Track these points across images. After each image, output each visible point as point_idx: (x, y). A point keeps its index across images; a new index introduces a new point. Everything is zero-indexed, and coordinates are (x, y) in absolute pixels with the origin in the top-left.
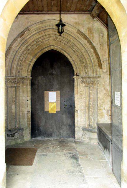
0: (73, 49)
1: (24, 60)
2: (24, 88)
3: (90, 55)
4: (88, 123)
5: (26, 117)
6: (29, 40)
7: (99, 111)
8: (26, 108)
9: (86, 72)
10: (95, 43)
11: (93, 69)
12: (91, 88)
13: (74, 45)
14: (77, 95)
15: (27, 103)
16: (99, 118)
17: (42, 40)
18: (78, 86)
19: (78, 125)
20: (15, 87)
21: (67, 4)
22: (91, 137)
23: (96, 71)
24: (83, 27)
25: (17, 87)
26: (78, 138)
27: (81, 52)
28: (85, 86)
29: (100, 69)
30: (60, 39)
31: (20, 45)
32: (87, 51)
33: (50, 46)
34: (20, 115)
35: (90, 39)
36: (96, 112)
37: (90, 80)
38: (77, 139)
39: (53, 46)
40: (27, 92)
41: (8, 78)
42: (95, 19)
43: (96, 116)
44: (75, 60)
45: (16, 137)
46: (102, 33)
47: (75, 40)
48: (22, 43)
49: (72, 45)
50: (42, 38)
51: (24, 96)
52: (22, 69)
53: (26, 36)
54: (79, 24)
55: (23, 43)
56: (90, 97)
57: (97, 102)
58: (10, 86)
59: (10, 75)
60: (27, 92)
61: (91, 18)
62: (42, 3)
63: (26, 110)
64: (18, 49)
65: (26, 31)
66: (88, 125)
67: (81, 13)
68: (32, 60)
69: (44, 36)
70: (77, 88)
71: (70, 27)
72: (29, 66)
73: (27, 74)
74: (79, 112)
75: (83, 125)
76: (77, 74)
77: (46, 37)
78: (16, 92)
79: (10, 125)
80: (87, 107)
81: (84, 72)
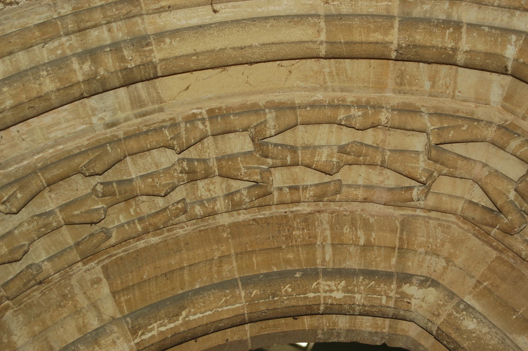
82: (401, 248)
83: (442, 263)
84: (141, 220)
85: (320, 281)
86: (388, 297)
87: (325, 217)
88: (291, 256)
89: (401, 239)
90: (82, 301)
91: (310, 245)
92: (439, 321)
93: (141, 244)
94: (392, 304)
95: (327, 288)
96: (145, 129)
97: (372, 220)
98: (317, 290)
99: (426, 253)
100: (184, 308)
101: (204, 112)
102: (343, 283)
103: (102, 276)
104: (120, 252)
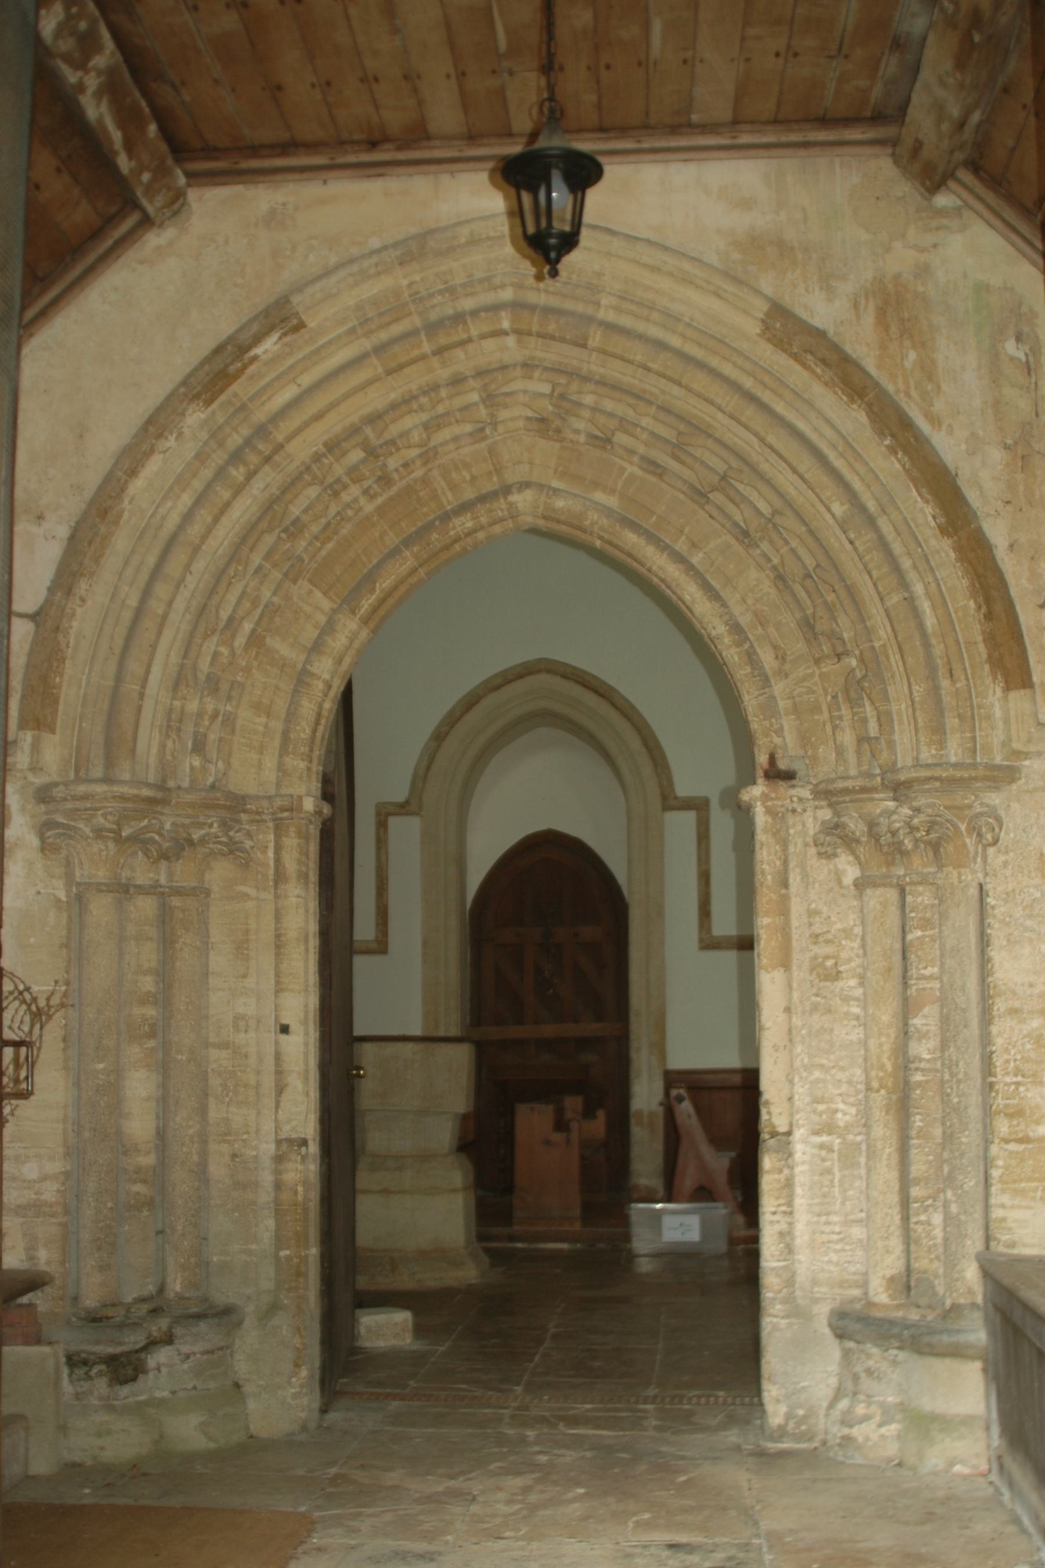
0: (731, 509)
1: (247, 627)
2: (250, 904)
3: (906, 564)
4: (892, 1264)
5: (265, 1196)
6: (287, 426)
7: (1003, 1126)
8: (269, 1102)
9: (862, 739)
10: (950, 430)
11: (939, 702)
12: (922, 898)
13: (735, 463)
14: (778, 975)
15: (278, 1056)
16: (1005, 1199)
17: (426, 426)
18: (785, 884)
19: (790, 1282)
20: (152, 889)
21: (646, 27)
22: (928, 1404)
23: (969, 720)
24: (827, 283)
25: (179, 892)
26: (789, 1416)
27: (811, 532)
28: (860, 885)
29: (1007, 689)
30: (602, 420)
31: (207, 473)
32: (871, 522)
33: (506, 490)
34: (201, 1172)
35: (902, 400)
36: (969, 1139)
37: (906, 811)
38: (781, 1433)
39: (529, 495)
40: (279, 944)
41: (82, 789)
42: (943, 200)
43: (971, 1183)
44: (761, 620)
45: (166, 1394)
46: (1019, 339)
47: (749, 412)
48: (219, 458)
49: (721, 467)
50: (421, 408)
51: (250, 982)
52: (229, 722)
53: (264, 389)
54: (783, 248)
55: (236, 457)
56: (912, 991)
57: (986, 1039)
58: (102, 875)
59: (110, 762)
60: (279, 944)
61: (905, 188)
62: (395, 31)
63: (268, 1126)
64: (188, 517)
65: (257, 340)
66: (892, 1280)
67: (794, 137)
68: (329, 628)
69: (443, 393)
70: (783, 909)
71: (687, 281)
72: (296, 691)
73: (280, 767)
74: (802, 1148)
75: (842, 1284)
76: (782, 765)
77: (459, 402)
78: (167, 943)
79: (103, 1268)
80: (879, 1099)
81: (847, 738)
82: (495, 470)
83: (527, 467)
84: (316, 538)
85: (453, 520)
86: (502, 510)
87: (435, 473)
88: (425, 510)
89: (493, 464)
90: (308, 609)
91: (435, 497)
92: (541, 509)
93: (323, 553)
94: (506, 513)
95: (460, 523)
96: (289, 480)
97: (468, 460)
98: (454, 528)
99: (514, 465)
100: (375, 582)
101: (321, 446)
102: (469, 515)
103: (311, 587)
104: (314, 565)
